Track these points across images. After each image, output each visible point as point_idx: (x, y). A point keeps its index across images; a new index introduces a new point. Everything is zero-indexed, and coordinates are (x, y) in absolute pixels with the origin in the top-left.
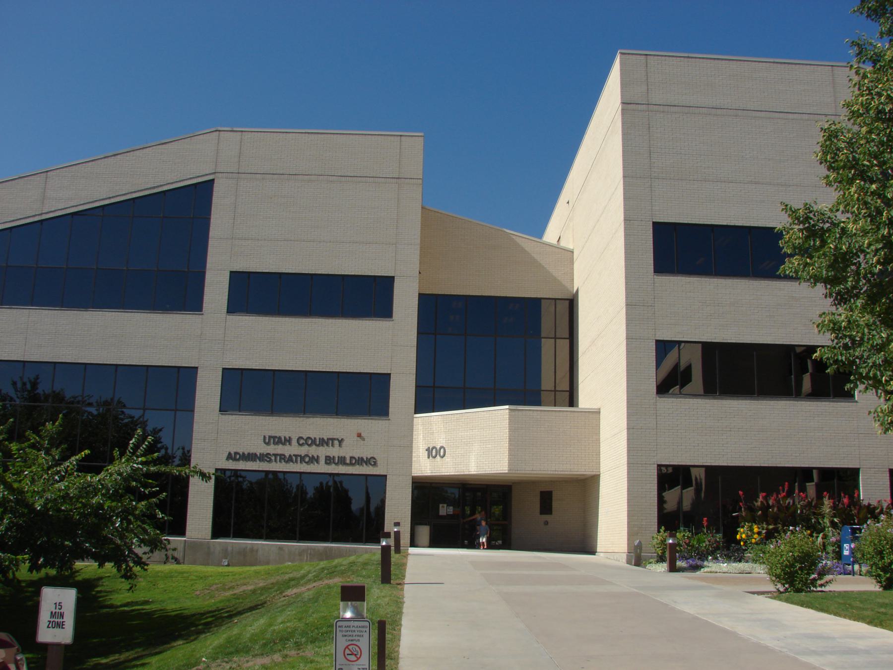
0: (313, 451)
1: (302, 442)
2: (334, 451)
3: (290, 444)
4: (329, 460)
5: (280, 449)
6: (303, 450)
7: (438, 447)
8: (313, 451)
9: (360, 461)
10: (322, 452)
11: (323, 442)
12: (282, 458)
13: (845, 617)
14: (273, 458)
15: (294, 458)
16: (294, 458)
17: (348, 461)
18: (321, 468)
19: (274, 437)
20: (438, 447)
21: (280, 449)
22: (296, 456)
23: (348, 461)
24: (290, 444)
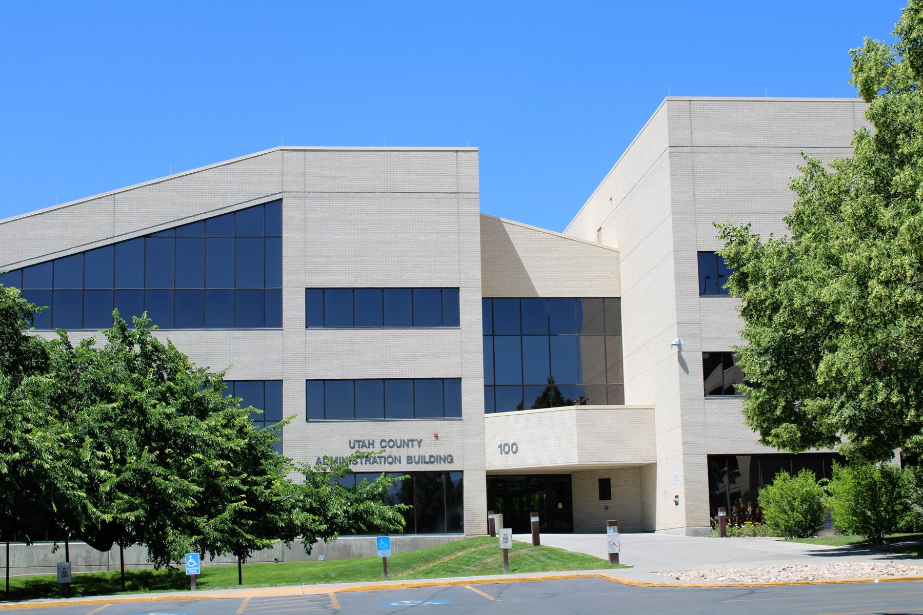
0: (395, 452)
1: (384, 444)
2: (414, 451)
8: (395, 452)
10: (403, 453)
11: (404, 444)
16: (378, 460)
23: (427, 460)
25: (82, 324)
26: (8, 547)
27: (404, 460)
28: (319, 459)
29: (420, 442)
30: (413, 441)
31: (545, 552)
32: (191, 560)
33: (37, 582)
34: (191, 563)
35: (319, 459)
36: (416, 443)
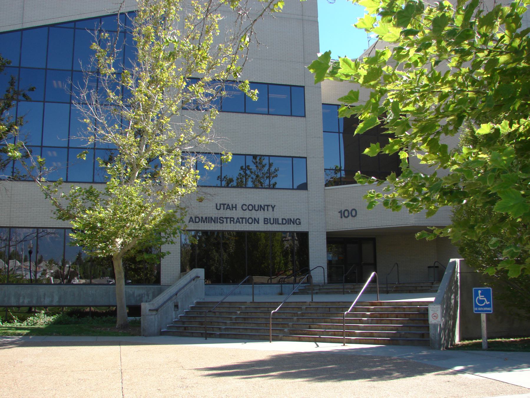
0: (255, 214)
1: (244, 207)
2: (269, 214)
3: (258, 223)
4: (266, 221)
5: (228, 213)
6: (247, 214)
7: (350, 217)
8: (255, 214)
9: (290, 221)
10: (261, 215)
11: (261, 208)
12: (232, 219)
13: (113, 336)
14: (225, 220)
15: (241, 220)
16: (241, 220)
17: (280, 222)
18: (261, 227)
19: (224, 205)
20: (350, 217)
21: (228, 213)
22: (242, 218)
23: (280, 222)
24: (258, 223)
25: (393, 112)
26: (282, 287)
27: (261, 221)
28: (191, 218)
29: (273, 208)
30: (268, 206)
31: (329, 359)
32: (480, 297)
33: (380, 378)
34: (482, 302)
35: (191, 218)
36: (270, 208)
